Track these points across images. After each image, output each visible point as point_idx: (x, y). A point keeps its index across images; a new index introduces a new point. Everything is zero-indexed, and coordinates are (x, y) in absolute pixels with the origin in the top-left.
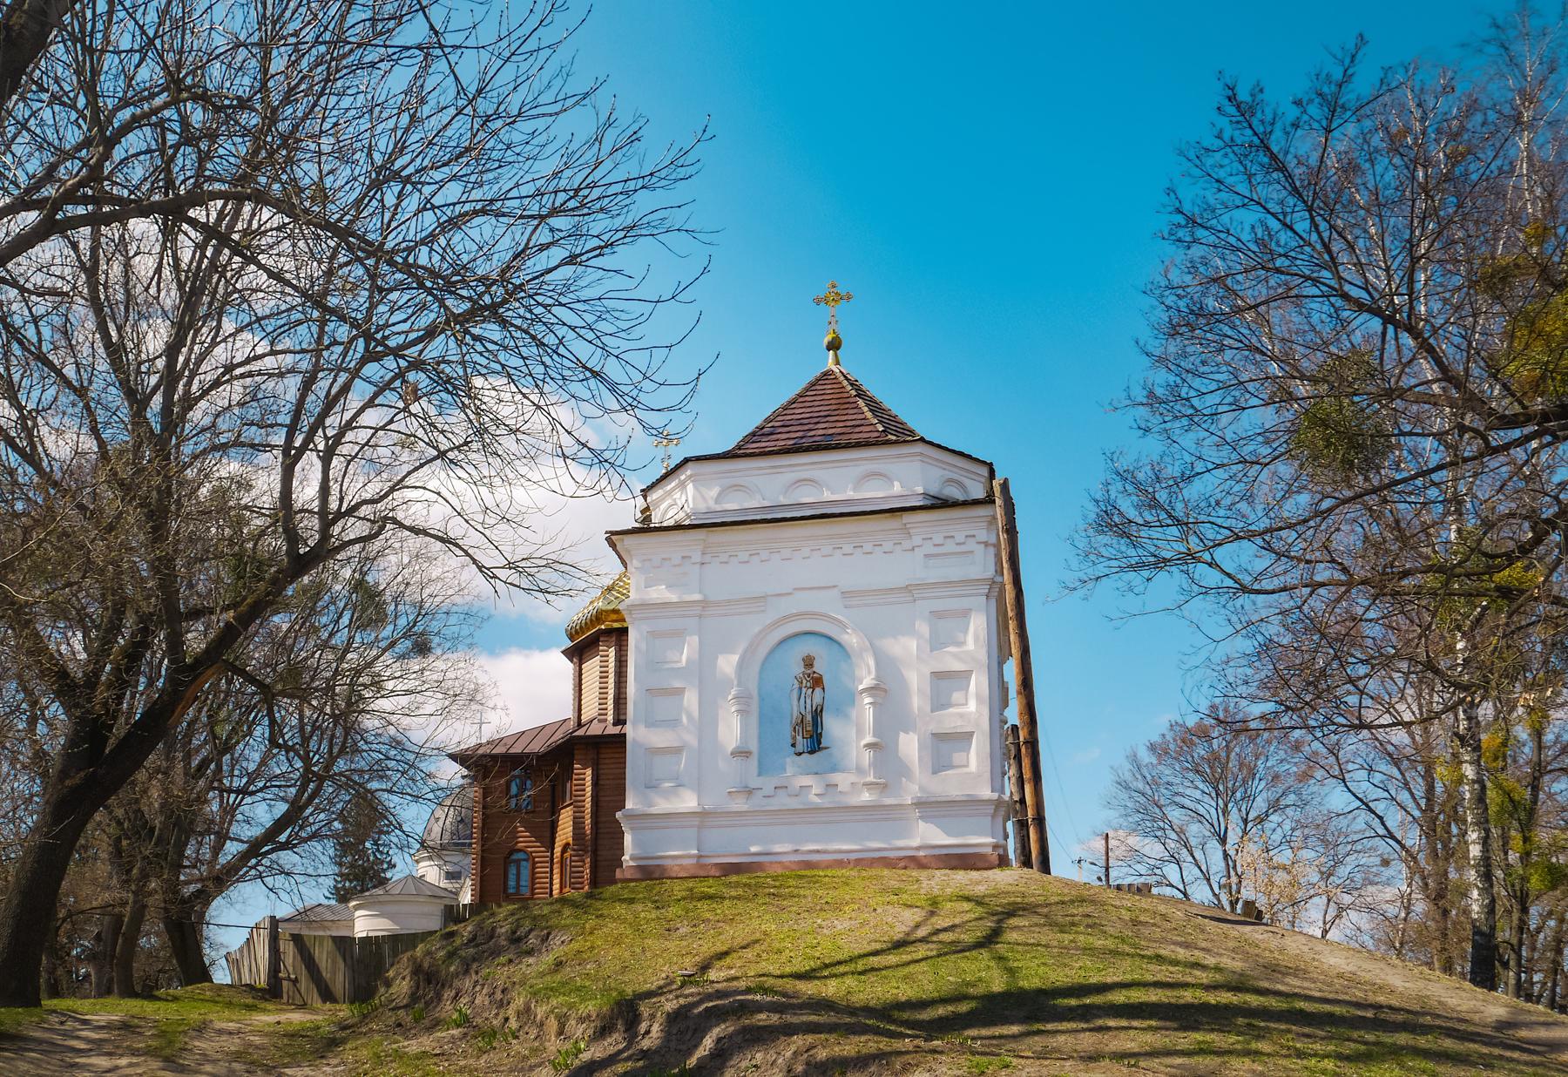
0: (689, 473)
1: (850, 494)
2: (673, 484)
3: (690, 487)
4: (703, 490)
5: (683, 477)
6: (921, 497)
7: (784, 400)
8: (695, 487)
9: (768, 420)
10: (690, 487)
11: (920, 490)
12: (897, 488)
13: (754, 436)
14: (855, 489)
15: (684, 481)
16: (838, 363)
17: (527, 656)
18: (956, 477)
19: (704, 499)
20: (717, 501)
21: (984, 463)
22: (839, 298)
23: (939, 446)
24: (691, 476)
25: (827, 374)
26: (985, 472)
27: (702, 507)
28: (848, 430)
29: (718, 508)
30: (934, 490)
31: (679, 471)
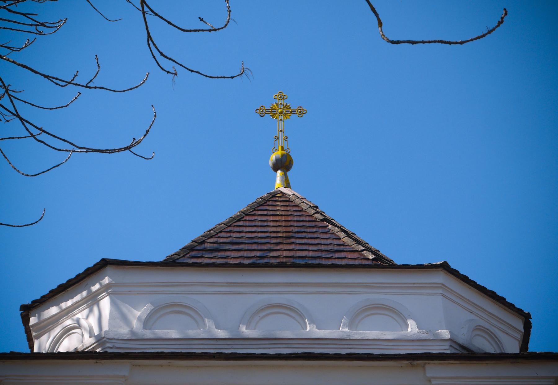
0: (106, 280)
1: (344, 331)
2: (78, 298)
3: (106, 303)
4: (126, 308)
5: (97, 287)
6: (448, 344)
7: (234, 211)
8: (113, 303)
9: (209, 235)
10: (106, 303)
11: (445, 334)
12: (412, 328)
13: (189, 249)
14: (351, 325)
15: (98, 292)
16: (287, 185)
17: (252, 234)
18: (487, 325)
19: (125, 319)
20: (147, 322)
21: (519, 312)
22: (288, 111)
23: (465, 279)
24: (108, 286)
25: (274, 197)
26: (519, 325)
27: (124, 331)
28: (324, 255)
29: (148, 334)
30: (463, 339)
31: (88, 280)
